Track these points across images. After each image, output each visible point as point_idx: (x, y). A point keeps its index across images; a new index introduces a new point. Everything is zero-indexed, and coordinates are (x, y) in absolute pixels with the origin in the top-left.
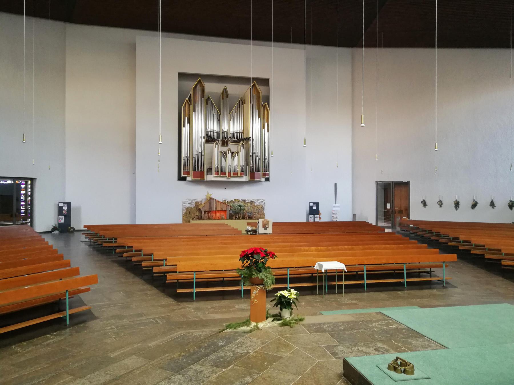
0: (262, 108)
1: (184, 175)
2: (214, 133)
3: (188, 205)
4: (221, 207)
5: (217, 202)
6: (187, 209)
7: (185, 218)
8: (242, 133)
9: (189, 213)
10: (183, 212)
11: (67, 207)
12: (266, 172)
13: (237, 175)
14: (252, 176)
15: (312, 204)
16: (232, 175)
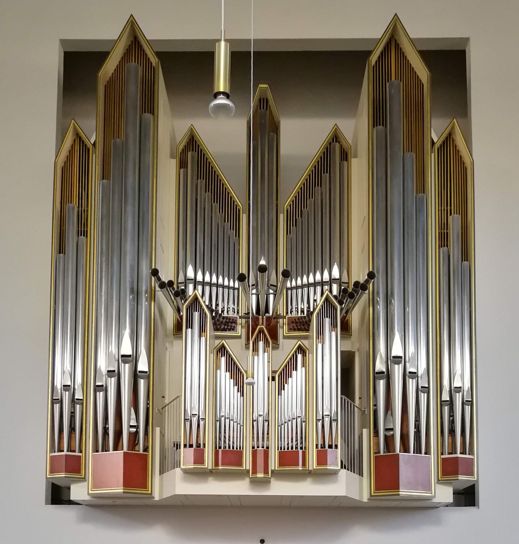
12: (459, 455)
13: (304, 464)
16: (274, 463)
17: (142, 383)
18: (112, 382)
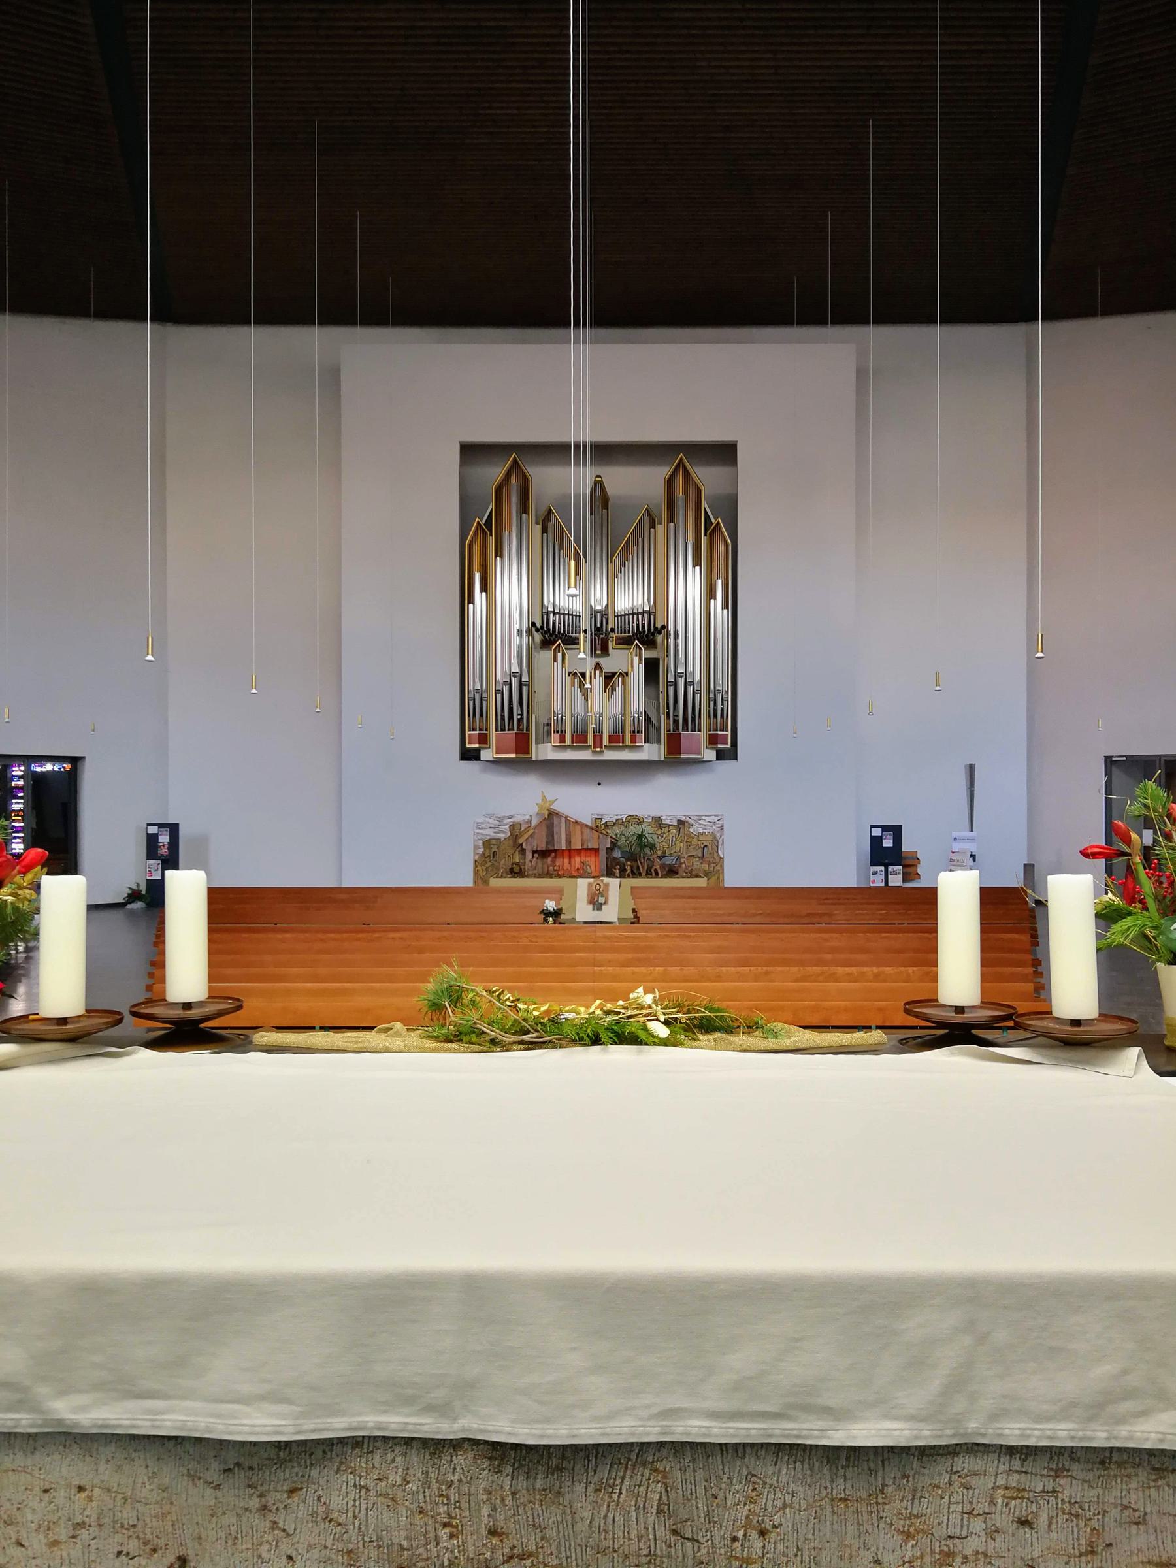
0: (705, 535)
1: (727, 744)
2: (571, 617)
3: (489, 833)
4: (582, 840)
5: (572, 824)
6: (487, 843)
7: (481, 871)
8: (652, 614)
9: (493, 857)
10: (475, 854)
11: (168, 837)
12: (719, 732)
13: (623, 743)
14: (674, 745)
15: (157, 827)
16: (605, 742)
17: (525, 688)
18: (506, 689)
